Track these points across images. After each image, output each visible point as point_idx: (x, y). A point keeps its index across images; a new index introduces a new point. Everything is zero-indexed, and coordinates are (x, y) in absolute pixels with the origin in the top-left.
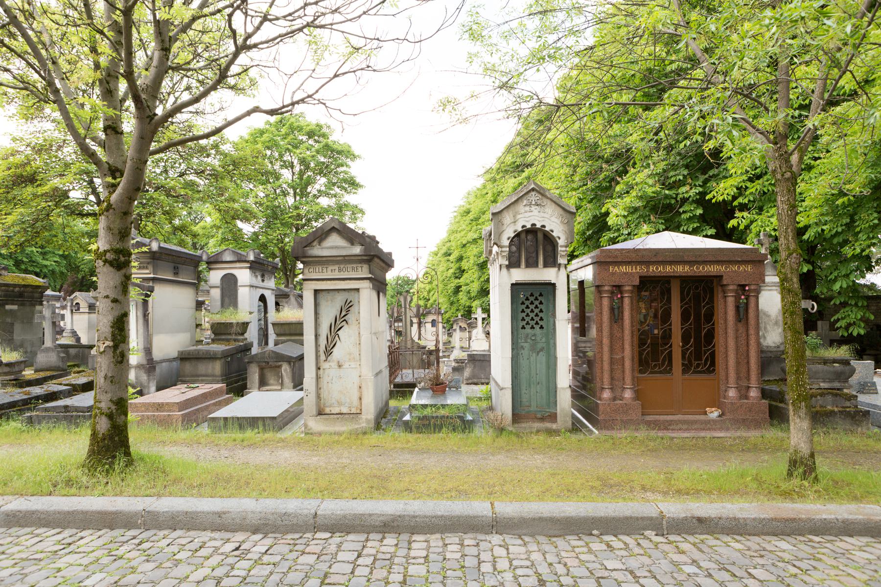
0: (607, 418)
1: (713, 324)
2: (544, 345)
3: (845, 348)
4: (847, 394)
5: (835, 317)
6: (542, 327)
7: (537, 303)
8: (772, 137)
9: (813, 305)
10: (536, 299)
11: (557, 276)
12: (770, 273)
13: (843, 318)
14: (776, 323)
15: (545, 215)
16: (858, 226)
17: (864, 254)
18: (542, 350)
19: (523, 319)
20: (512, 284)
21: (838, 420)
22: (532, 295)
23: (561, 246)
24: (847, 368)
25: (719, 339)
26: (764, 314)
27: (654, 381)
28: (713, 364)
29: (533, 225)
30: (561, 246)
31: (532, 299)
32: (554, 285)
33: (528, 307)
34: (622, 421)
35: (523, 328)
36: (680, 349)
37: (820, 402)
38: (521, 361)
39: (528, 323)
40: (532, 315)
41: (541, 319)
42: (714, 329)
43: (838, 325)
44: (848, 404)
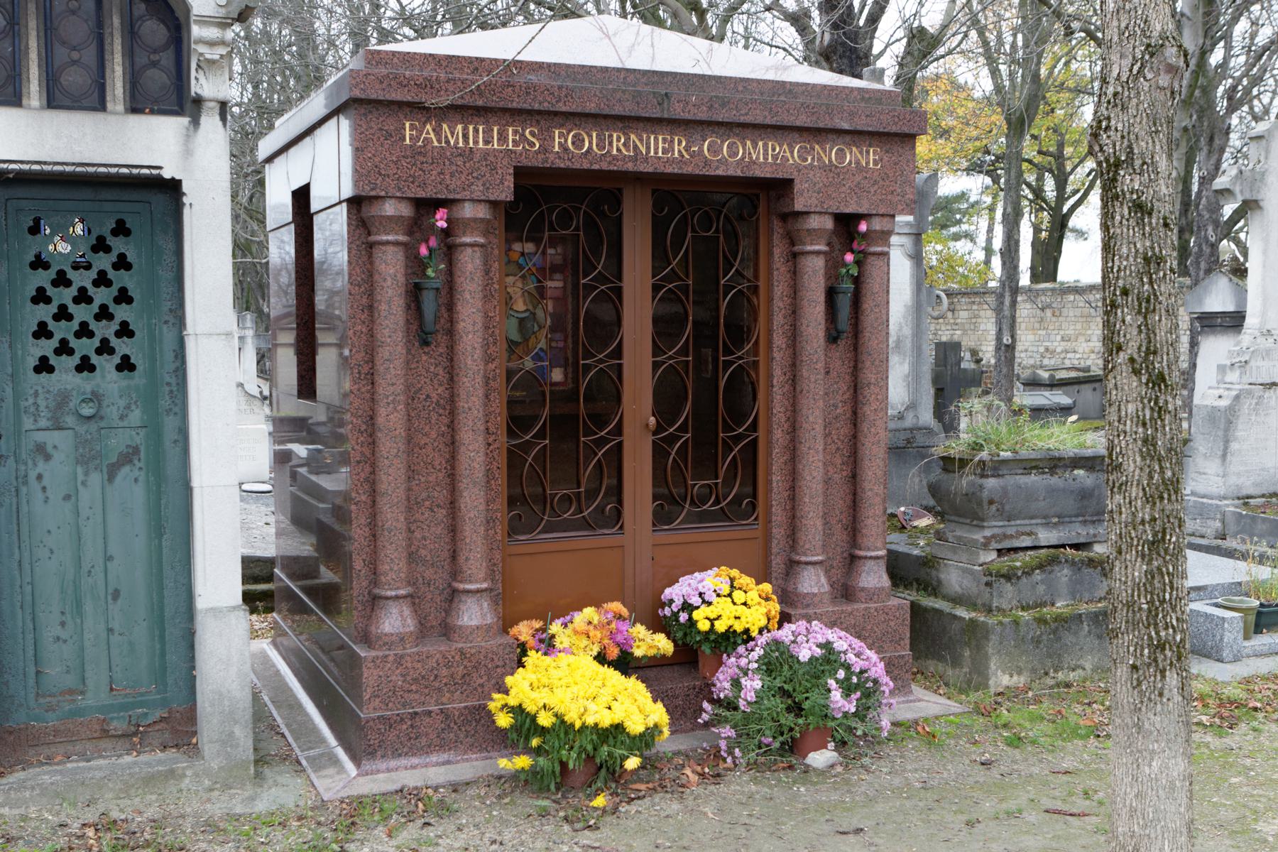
6: (126, 365)
11: (188, 152)
18: (128, 457)
30: (205, 21)
32: (173, 188)
35: (44, 366)
40: (81, 313)
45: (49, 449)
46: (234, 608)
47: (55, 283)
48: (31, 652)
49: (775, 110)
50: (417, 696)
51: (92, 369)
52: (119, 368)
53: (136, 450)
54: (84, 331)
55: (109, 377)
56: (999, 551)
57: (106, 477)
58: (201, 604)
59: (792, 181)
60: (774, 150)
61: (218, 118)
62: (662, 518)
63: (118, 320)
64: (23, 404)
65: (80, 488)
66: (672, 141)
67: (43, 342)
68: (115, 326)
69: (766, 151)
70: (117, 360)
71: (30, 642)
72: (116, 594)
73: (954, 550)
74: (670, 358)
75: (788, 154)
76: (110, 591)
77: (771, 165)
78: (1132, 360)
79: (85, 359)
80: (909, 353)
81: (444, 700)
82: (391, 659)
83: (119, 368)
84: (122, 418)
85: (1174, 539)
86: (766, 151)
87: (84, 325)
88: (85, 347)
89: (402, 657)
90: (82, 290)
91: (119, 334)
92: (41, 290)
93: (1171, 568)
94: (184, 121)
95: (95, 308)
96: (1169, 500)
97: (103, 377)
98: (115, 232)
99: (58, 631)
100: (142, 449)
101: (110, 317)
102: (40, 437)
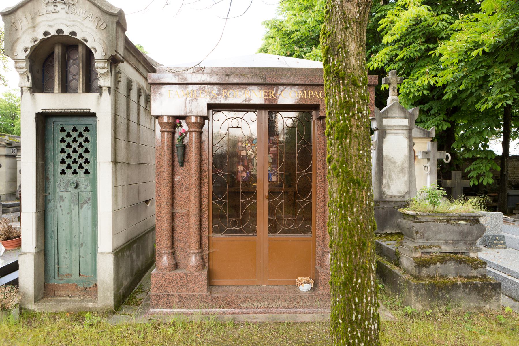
0: (161, 293)
1: (310, 170)
2: (90, 196)
3: (473, 200)
4: (474, 260)
5: (468, 169)
6: (87, 172)
7: (81, 140)
8: (497, 238)
9: (447, 156)
10: (81, 135)
11: (98, 104)
12: (397, 116)
13: (474, 170)
14: (402, 171)
15: (76, 18)
16: (492, 80)
17: (496, 107)
18: (86, 202)
19: (63, 162)
20: (38, 114)
21: (460, 294)
22: (75, 130)
23: (99, 61)
24: (475, 227)
25: (317, 190)
26: (389, 160)
27: (227, 244)
28: (309, 220)
29: (59, 31)
30: (99, 61)
31: (75, 135)
32: (94, 115)
33: (69, 146)
34: (180, 297)
35: (63, 172)
36: (267, 202)
37: (440, 271)
38: (60, 216)
39: (69, 167)
40: (74, 156)
41: (87, 161)
42: (310, 176)
43: (470, 175)
44: (474, 273)
45: (64, 198)
46: (109, 253)
47: (67, 147)
48: (56, 261)
49: (309, 78)
50: (170, 289)
51: (77, 173)
52: (85, 173)
53: (89, 199)
54: (75, 162)
55: (81, 176)
56: (422, 253)
57: (80, 207)
58: (99, 250)
59: (319, 105)
60: (311, 94)
61: (108, 92)
62: (273, 229)
63: (85, 158)
64: (57, 184)
65: (72, 210)
66: (269, 92)
67: (63, 165)
68: (84, 160)
69: (307, 94)
70: (84, 170)
71: (56, 257)
72: (82, 244)
73: (405, 250)
74: (304, 172)
75: (317, 95)
76: (80, 243)
77: (310, 99)
78: (335, 169)
79: (75, 170)
80: (407, 173)
81: (180, 291)
82: (161, 275)
83: (85, 173)
84: (85, 189)
85: (359, 281)
86: (307, 94)
87: (75, 159)
88: (75, 166)
89: (165, 274)
90: (75, 149)
91: (85, 163)
92: (63, 149)
93: (357, 300)
94: (98, 94)
95: (78, 154)
96: (356, 255)
97: (80, 176)
98: (85, 131)
99: (65, 255)
100: (91, 199)
101: (83, 157)
102: (61, 194)
